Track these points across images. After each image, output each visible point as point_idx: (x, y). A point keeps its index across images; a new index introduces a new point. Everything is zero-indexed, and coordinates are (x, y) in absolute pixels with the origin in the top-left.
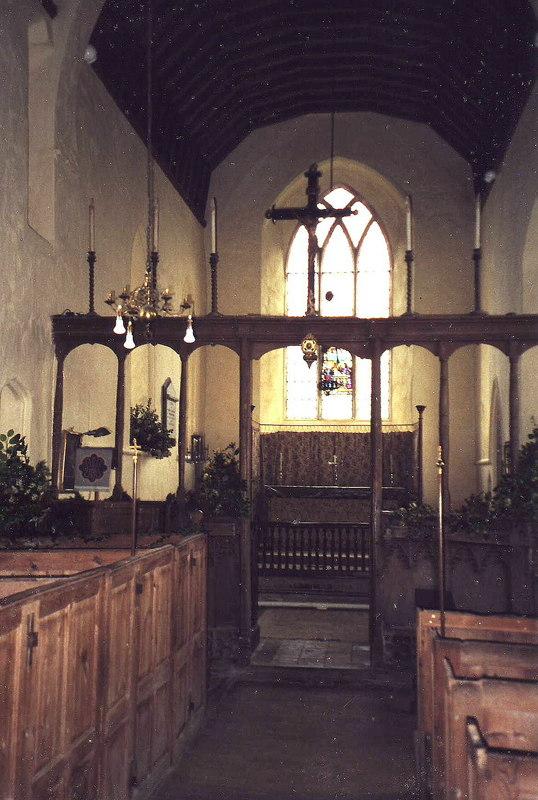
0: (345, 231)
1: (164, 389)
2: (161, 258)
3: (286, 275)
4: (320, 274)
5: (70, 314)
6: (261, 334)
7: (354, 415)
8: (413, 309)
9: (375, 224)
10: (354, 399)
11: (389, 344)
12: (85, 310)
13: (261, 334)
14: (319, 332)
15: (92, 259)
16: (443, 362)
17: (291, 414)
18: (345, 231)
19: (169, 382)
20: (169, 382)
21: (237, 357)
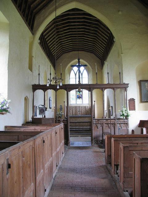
0: (73, 70)
1: (49, 99)
2: (62, 74)
3: (70, 79)
4: (82, 78)
5: (35, 84)
6: (69, 88)
7: (82, 103)
8: (81, 82)
9: (85, 70)
10: (82, 100)
11: (94, 88)
12: (38, 84)
13: (69, 88)
14: (79, 87)
15: (61, 74)
16: (56, 92)
17: (77, 103)
18: (73, 70)
19: (50, 97)
20: (50, 97)
21: (66, 91)
